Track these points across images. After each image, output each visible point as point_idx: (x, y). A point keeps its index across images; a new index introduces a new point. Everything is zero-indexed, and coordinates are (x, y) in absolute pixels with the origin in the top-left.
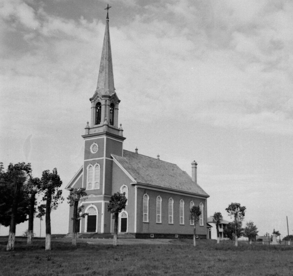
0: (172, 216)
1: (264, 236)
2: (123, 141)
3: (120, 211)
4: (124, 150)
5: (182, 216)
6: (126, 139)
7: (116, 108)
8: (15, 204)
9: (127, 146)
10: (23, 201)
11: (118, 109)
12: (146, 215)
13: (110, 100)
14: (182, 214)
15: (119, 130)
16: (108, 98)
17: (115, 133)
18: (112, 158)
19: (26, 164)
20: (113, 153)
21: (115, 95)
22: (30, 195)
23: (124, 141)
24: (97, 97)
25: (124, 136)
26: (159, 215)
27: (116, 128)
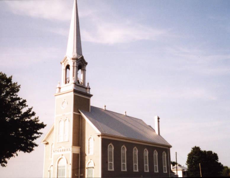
0: (137, 164)
1: (20, 151)
2: (90, 98)
3: (29, 151)
4: (91, 107)
5: (124, 162)
6: (93, 96)
7: (84, 69)
8: (29, 142)
9: (94, 102)
10: (221, 172)
11: (85, 70)
12: (111, 163)
13: (78, 62)
14: (156, 163)
15: (86, 88)
16: (76, 61)
17: (83, 90)
18: (80, 113)
19: (18, 84)
20: (80, 110)
21: (82, 58)
22: (3, 160)
23: (92, 97)
24: (67, 60)
25: (91, 93)
26: (136, 164)
27: (84, 86)
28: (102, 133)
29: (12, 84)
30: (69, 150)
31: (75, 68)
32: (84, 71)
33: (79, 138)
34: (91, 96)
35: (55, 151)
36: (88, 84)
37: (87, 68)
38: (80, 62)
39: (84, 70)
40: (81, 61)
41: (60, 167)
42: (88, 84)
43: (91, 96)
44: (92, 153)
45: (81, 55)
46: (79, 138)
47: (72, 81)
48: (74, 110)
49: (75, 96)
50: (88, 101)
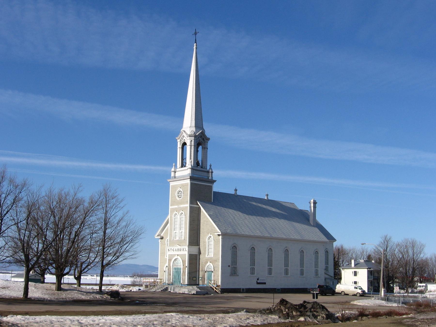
4: (215, 193)
15: (208, 172)
28: (229, 231)
29: (245, 310)
30: (185, 250)
31: (193, 147)
32: (206, 149)
33: (195, 238)
34: (213, 182)
35: (170, 250)
36: (210, 166)
37: (210, 144)
38: (200, 139)
39: (205, 149)
40: (201, 137)
41: (104, 285)
42: (210, 166)
43: (213, 182)
44: (51, 318)
45: (202, 128)
46: (195, 238)
47: (189, 162)
48: (191, 203)
49: (191, 184)
50: (211, 187)
